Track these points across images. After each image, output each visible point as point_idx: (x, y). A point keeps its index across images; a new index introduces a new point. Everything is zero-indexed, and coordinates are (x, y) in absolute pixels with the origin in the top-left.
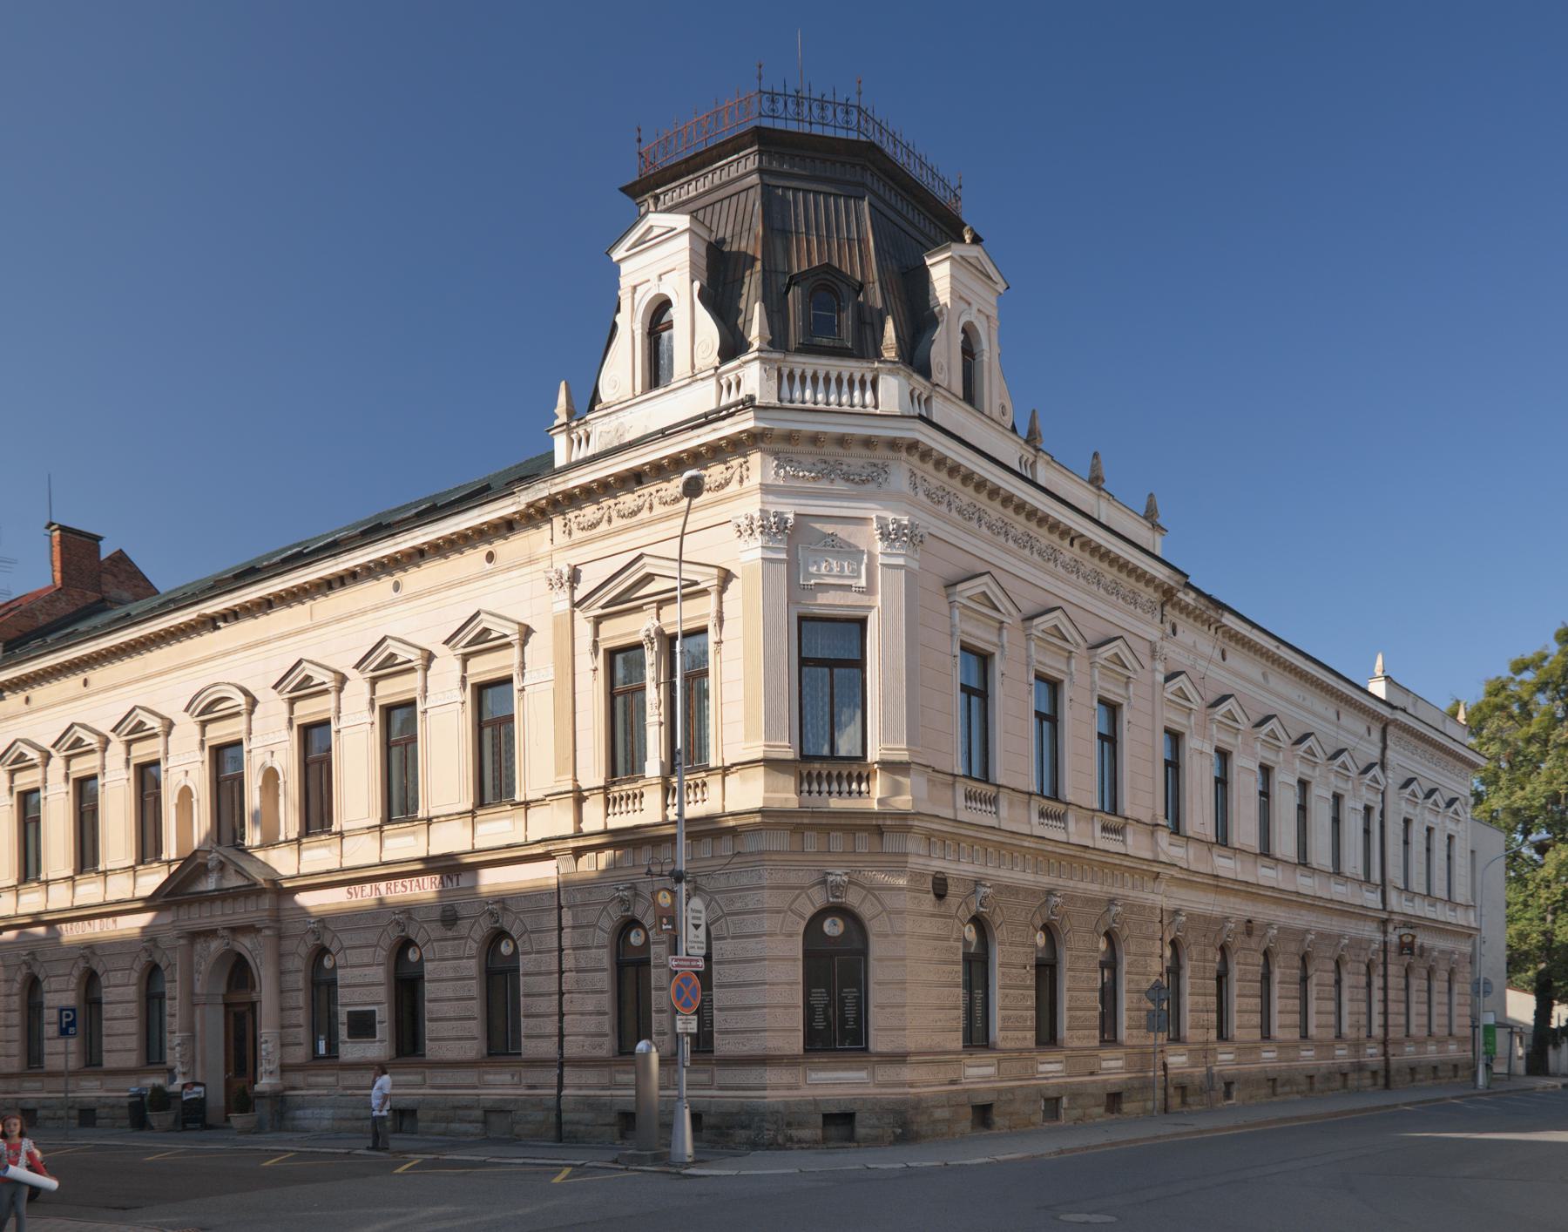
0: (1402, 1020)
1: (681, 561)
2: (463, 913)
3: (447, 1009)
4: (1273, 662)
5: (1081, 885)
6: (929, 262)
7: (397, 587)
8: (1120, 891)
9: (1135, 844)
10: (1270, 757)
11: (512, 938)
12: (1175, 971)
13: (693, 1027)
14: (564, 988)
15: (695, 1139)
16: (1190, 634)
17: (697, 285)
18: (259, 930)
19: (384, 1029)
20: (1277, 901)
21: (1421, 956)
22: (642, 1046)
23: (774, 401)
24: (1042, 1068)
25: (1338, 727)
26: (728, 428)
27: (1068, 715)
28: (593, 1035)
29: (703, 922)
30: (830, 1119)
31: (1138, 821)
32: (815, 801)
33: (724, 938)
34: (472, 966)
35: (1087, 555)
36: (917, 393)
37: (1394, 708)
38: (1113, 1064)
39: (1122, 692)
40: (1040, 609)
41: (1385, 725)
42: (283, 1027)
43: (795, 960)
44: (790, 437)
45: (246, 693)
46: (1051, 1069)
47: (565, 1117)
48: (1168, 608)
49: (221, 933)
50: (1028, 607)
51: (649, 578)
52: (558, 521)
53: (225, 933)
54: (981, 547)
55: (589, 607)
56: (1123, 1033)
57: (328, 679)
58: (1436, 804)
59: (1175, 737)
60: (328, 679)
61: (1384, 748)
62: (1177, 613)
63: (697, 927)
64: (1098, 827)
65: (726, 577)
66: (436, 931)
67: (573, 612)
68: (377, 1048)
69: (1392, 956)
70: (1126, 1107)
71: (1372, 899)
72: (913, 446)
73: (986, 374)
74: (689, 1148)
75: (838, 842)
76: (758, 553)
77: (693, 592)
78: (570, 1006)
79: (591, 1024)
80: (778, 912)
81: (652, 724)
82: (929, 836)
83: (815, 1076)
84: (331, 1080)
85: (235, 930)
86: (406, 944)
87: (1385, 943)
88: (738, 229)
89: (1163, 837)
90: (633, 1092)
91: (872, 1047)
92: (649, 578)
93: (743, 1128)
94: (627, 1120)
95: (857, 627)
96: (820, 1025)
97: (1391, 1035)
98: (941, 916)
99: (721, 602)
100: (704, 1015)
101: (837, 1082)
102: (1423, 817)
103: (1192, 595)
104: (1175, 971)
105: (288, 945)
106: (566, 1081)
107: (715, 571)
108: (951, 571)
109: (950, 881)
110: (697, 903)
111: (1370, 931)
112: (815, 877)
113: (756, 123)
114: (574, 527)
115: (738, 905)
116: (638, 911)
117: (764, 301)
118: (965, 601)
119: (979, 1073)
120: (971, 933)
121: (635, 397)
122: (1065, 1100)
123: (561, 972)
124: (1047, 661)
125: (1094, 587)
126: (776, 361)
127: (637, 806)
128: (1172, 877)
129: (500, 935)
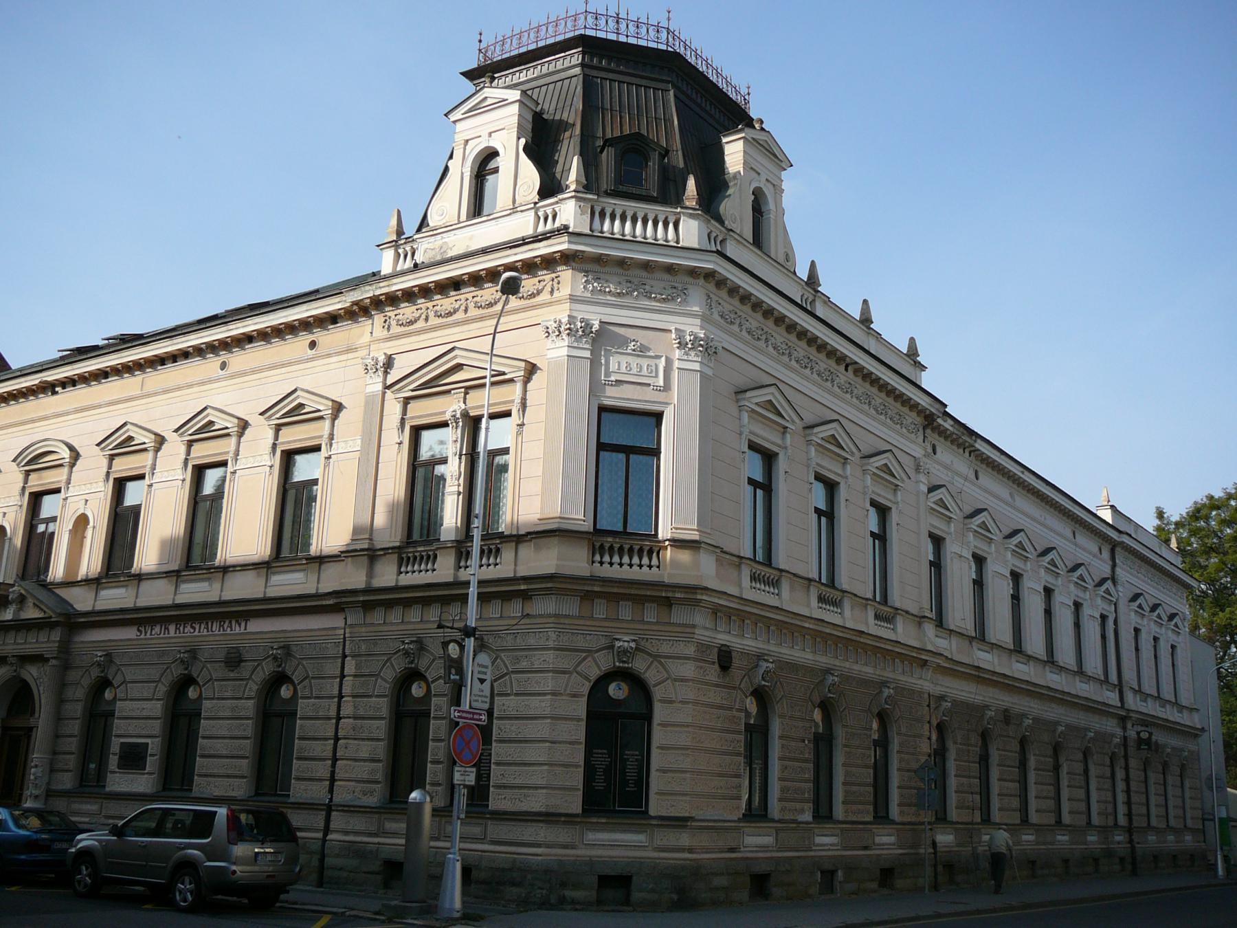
0: (1144, 810)
1: (492, 355)
2: (247, 656)
3: (220, 747)
4: (1019, 485)
5: (856, 667)
6: (724, 140)
7: (223, 366)
8: (891, 675)
9: (903, 632)
10: (1019, 565)
11: (292, 682)
12: (940, 753)
13: (471, 779)
14: (341, 734)
15: (464, 893)
16: (946, 454)
17: (523, 141)
18: (47, 660)
19: (152, 763)
20: (1030, 693)
21: (1157, 751)
22: (415, 795)
23: (588, 231)
24: (818, 840)
25: (1076, 545)
26: (543, 249)
27: (843, 513)
28: (364, 782)
29: (488, 677)
30: (606, 881)
31: (907, 612)
32: (606, 571)
33: (508, 695)
34: (249, 707)
35: (859, 380)
36: (713, 235)
37: (1120, 532)
38: (885, 839)
39: (890, 497)
40: (818, 420)
41: (1114, 546)
42: (55, 753)
43: (579, 720)
44: (599, 260)
45: (71, 448)
46: (826, 842)
47: (329, 861)
48: (928, 431)
49: (11, 660)
50: (809, 418)
51: (458, 367)
52: (378, 319)
53: (13, 660)
54: (769, 364)
55: (399, 390)
56: (894, 811)
57: (148, 440)
58: (1159, 617)
59: (937, 541)
60: (148, 440)
61: (1114, 566)
62: (936, 436)
63: (482, 681)
64: (871, 614)
65: (531, 369)
66: (218, 671)
67: (384, 394)
68: (142, 782)
69: (1132, 750)
70: (899, 883)
71: (1112, 698)
72: (709, 275)
73: (772, 229)
74: (458, 904)
75: (626, 611)
76: (565, 351)
77: (501, 380)
78: (342, 753)
79: (363, 770)
80: (564, 673)
81: (451, 493)
82: (716, 611)
83: (591, 836)
84: (94, 808)
85: (26, 659)
86: (188, 681)
87: (1125, 738)
88: (560, 105)
89: (930, 629)
90: (403, 841)
91: (652, 812)
92: (458, 367)
93: (514, 884)
94: (393, 870)
95: (653, 420)
96: (600, 785)
97: (1135, 824)
98: (725, 687)
99: (525, 391)
100: (482, 766)
101: (614, 844)
102: (1149, 628)
103: (950, 422)
104: (940, 753)
105: (73, 676)
106: (332, 826)
107: (523, 364)
108: (742, 382)
109: (734, 654)
110: (483, 658)
111: (1110, 726)
112: (603, 642)
113: (582, 32)
114: (393, 323)
115: (524, 664)
116: (422, 665)
117: (581, 154)
118: (753, 407)
119: (757, 842)
120: (752, 706)
121: (459, 222)
122: (840, 873)
123: (339, 718)
124: (824, 463)
125: (866, 407)
126: (590, 200)
127: (430, 566)
128: (939, 665)
129: (280, 679)
